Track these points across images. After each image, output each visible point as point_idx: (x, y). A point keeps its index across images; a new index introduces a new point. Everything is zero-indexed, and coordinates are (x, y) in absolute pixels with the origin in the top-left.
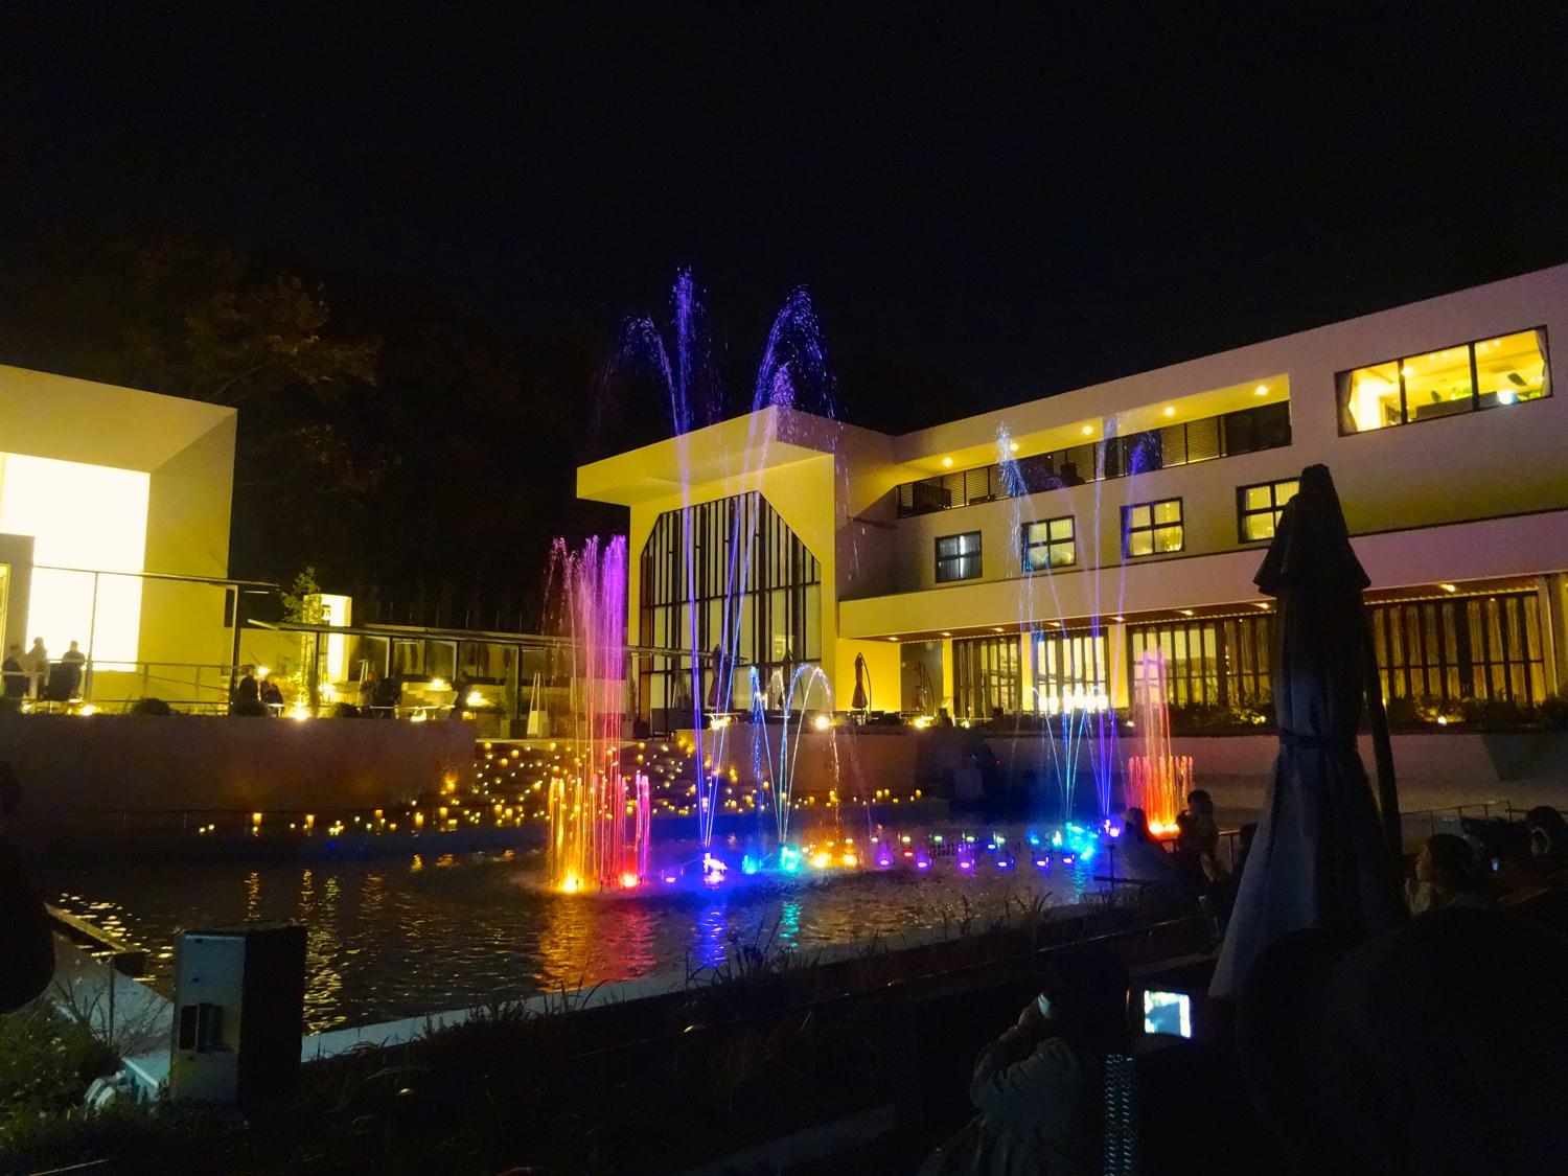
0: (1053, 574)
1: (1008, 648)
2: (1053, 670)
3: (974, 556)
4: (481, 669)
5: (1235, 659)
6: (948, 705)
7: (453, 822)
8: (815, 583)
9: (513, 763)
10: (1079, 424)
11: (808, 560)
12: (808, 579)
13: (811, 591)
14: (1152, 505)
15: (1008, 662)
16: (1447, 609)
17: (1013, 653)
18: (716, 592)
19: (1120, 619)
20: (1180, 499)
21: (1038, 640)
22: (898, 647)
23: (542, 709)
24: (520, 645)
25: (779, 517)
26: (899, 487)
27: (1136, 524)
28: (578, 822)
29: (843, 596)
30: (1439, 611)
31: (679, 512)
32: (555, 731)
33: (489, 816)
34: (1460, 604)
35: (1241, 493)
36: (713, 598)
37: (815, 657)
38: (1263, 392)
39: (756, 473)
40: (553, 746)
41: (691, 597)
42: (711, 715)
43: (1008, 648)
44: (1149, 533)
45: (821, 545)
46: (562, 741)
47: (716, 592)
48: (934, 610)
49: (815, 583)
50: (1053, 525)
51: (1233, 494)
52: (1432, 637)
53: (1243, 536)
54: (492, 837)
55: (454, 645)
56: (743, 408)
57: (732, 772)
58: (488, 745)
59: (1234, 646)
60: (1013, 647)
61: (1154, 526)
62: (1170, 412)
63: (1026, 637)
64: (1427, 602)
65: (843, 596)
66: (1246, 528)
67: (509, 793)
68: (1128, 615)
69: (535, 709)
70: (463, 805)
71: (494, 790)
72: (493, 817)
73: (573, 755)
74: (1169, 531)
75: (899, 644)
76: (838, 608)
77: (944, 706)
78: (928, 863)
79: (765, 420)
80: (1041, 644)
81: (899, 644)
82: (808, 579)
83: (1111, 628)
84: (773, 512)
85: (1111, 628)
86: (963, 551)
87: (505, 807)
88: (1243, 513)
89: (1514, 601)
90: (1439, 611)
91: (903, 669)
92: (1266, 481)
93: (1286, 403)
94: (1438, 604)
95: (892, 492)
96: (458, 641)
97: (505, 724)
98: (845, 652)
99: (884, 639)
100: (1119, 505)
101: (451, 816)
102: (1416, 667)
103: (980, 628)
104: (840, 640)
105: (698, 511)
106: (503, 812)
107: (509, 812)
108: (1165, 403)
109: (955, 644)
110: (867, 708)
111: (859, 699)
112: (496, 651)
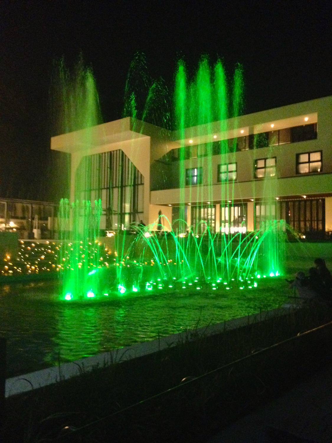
0: (256, 181)
1: (271, 208)
2: (227, 218)
3: (200, 175)
4: (13, 213)
5: (292, 215)
6: (189, 229)
7: (11, 272)
8: (142, 184)
9: (33, 250)
10: (269, 123)
11: (140, 175)
12: (139, 182)
13: (140, 187)
14: (309, 153)
15: (211, 215)
16: (303, 203)
17: (213, 212)
18: (116, 185)
19: (252, 200)
20: (275, 157)
21: (231, 206)
22: (171, 208)
23: (38, 228)
24: (32, 204)
25: (129, 159)
26: (173, 150)
27: (259, 166)
28: (249, 272)
29: (154, 188)
30: (299, 204)
31: (101, 155)
32: (43, 236)
33: (25, 270)
34: (305, 201)
35: (298, 156)
36: (140, 184)
37: (142, 211)
38: (306, 120)
39: (131, 140)
40: (48, 242)
41: (130, 184)
42: (107, 232)
43: (271, 208)
44: (308, 164)
45: (145, 172)
46: (51, 240)
47: (116, 185)
48: (182, 194)
49: (142, 184)
50: (312, 155)
51: (295, 157)
52: (302, 212)
53: (297, 173)
54: (23, 279)
55: (5, 203)
56: (120, 117)
57: (116, 253)
58: (22, 242)
59: (292, 212)
60: (258, 207)
61: (309, 162)
62: (272, 126)
63: (218, 206)
64: (290, 201)
65: (154, 188)
66: (298, 169)
67: (32, 260)
68: (173, 204)
69: (35, 228)
70: (14, 266)
71: (26, 259)
72: (27, 270)
73: (55, 246)
74: (271, 169)
75: (171, 207)
76: (150, 194)
77: (188, 230)
78: (200, 288)
79: (125, 121)
80: (223, 209)
81: (171, 207)
82: (139, 182)
83: (249, 203)
84: (127, 157)
85: (249, 203)
86: (196, 174)
87: (31, 266)
88: (298, 163)
89: (292, 203)
90: (299, 204)
91: (173, 216)
92: (306, 152)
93: (316, 124)
94: (300, 201)
95: (170, 152)
96: (7, 202)
97: (26, 234)
98: (153, 210)
99: (166, 205)
100: (296, 153)
101: (9, 269)
102: (309, 220)
103: (216, 201)
104: (151, 205)
105: (109, 154)
106: (31, 268)
107: (33, 268)
108: (271, 122)
109: (192, 208)
110: (162, 230)
111: (159, 228)
112: (19, 206)
